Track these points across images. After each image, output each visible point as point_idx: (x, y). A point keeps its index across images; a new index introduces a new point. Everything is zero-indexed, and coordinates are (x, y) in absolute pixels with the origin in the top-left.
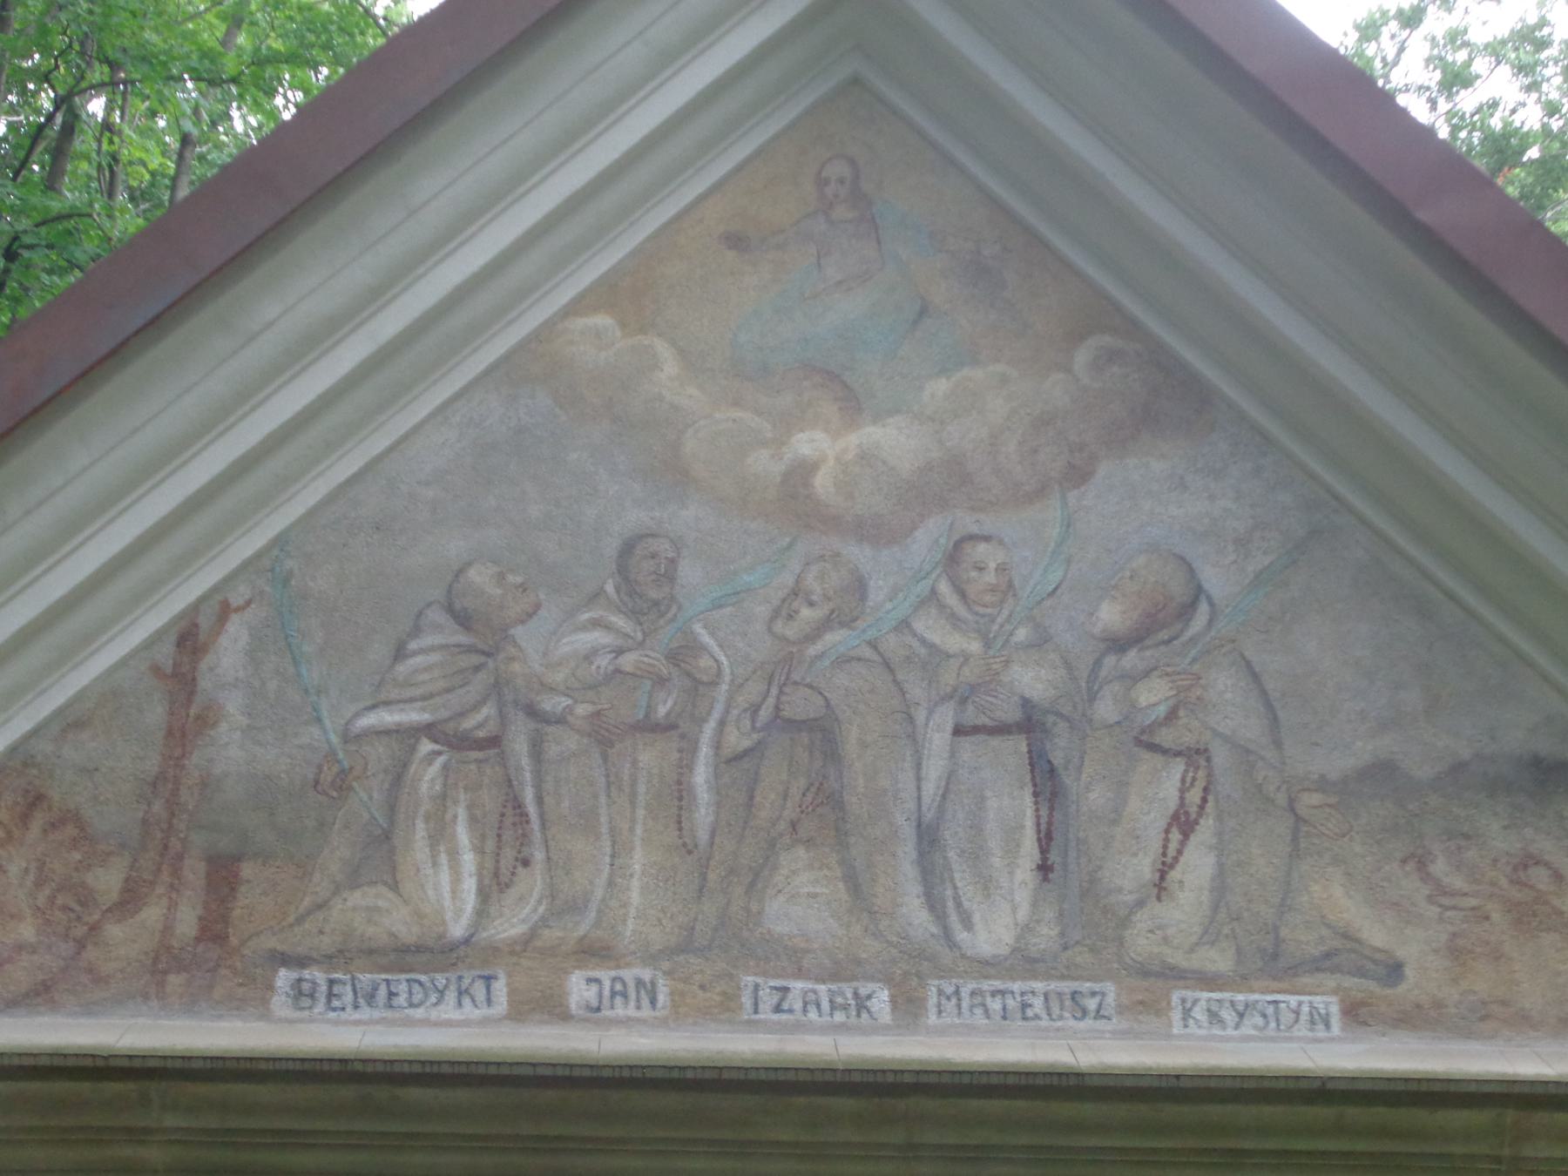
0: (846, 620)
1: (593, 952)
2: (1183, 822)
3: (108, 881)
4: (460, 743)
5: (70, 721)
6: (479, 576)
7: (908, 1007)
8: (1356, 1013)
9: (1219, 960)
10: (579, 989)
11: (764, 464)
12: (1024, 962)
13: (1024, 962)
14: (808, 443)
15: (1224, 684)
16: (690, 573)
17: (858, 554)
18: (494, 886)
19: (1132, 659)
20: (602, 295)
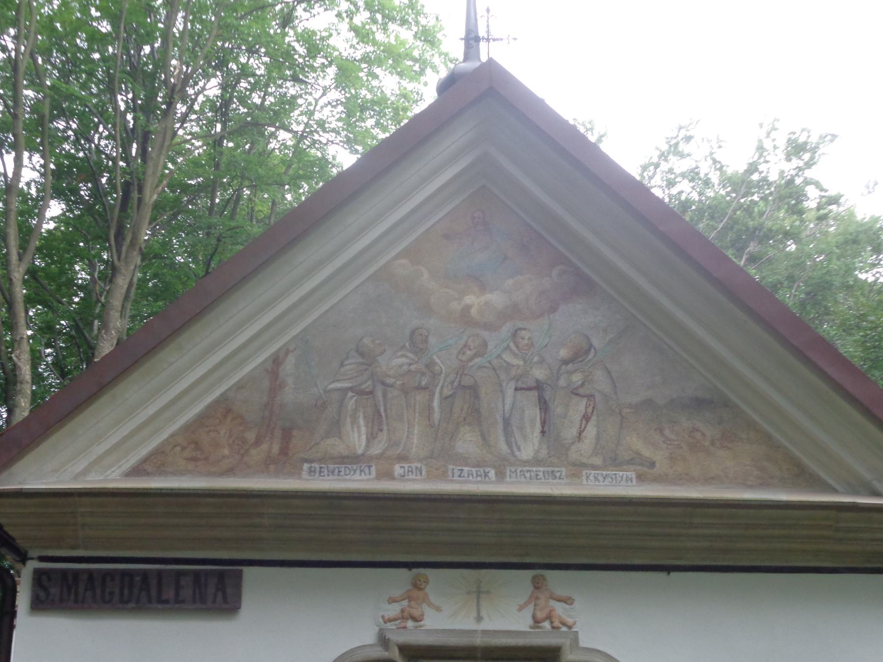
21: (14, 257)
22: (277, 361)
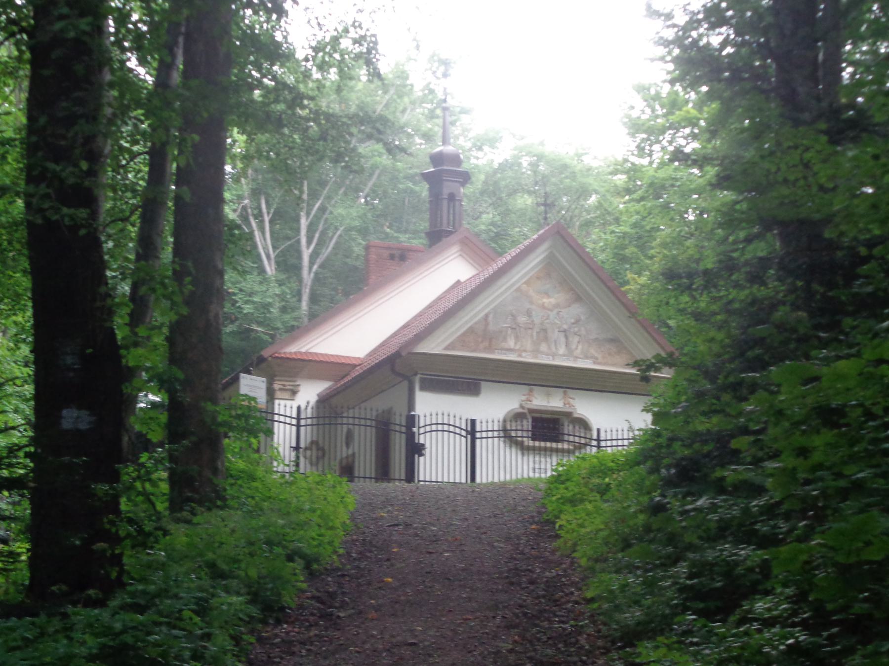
0: (547, 319)
1: (525, 351)
2: (579, 342)
3: (480, 340)
4: (513, 329)
5: (476, 323)
6: (514, 311)
7: (554, 359)
8: (594, 363)
9: (581, 356)
10: (524, 354)
11: (540, 302)
12: (564, 355)
13: (564, 355)
14: (545, 300)
15: (583, 329)
16: (534, 313)
17: (549, 312)
18: (516, 343)
19: (574, 325)
20: (525, 283)
21: (304, 241)
22: (487, 316)
